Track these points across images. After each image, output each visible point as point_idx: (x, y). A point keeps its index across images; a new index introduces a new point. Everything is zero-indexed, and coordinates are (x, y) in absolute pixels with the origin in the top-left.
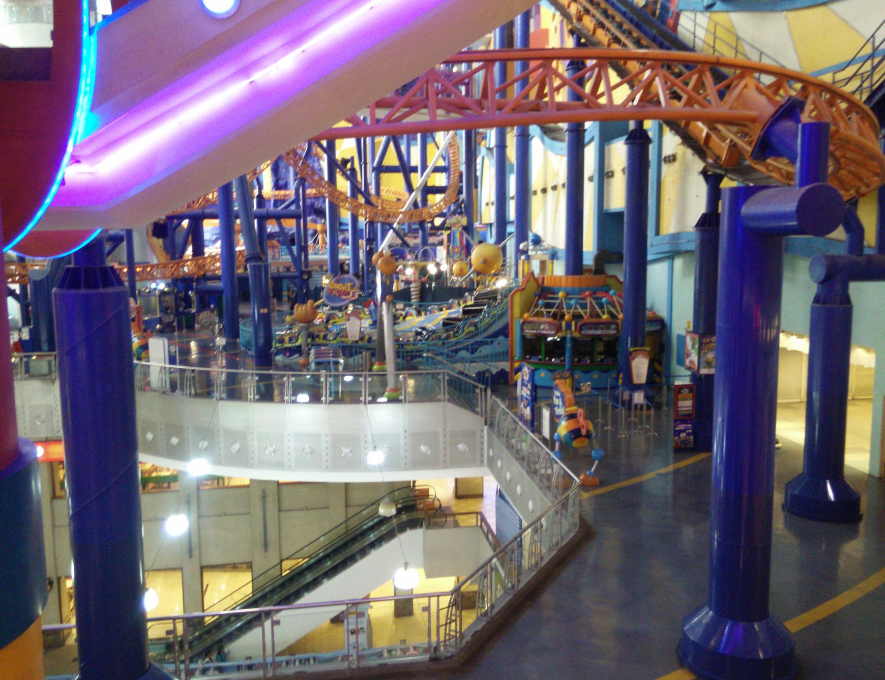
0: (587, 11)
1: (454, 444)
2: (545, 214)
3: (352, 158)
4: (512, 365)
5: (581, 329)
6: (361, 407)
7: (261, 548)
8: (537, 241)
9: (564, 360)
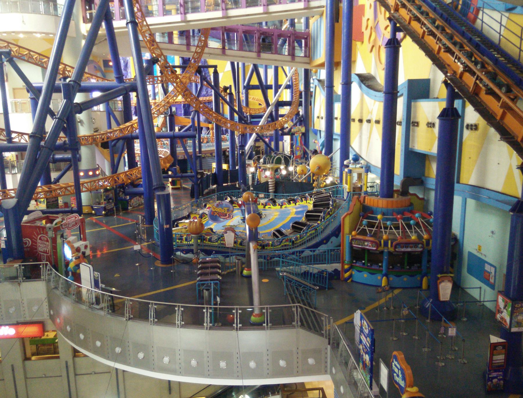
0: (404, 6)
1: (305, 359)
2: (361, 137)
3: (231, 86)
4: (343, 267)
5: (395, 247)
6: (234, 332)
7: (166, 391)
8: (357, 159)
9: (381, 266)
